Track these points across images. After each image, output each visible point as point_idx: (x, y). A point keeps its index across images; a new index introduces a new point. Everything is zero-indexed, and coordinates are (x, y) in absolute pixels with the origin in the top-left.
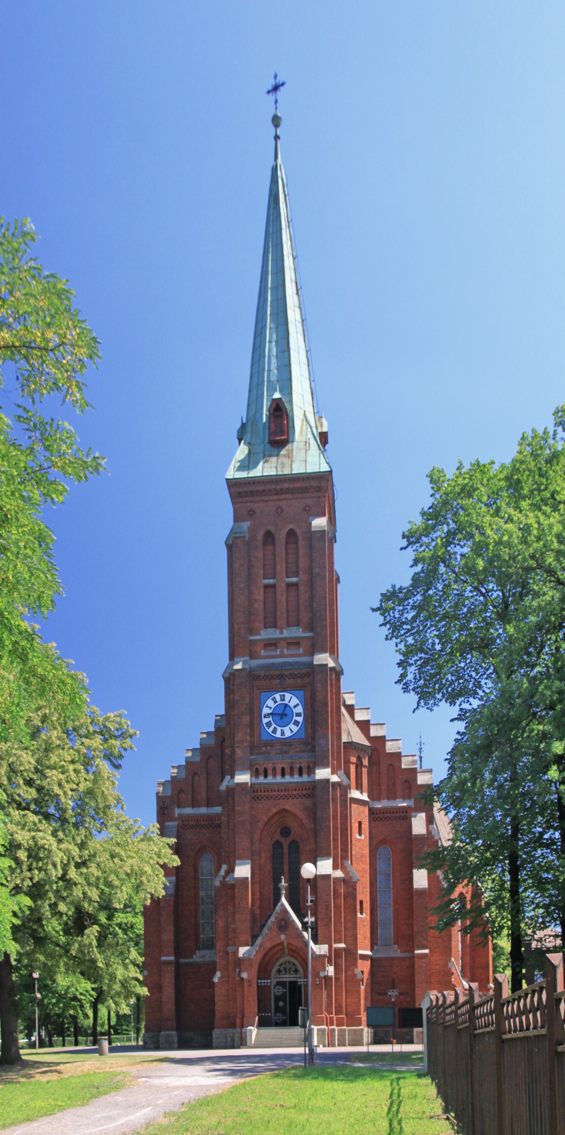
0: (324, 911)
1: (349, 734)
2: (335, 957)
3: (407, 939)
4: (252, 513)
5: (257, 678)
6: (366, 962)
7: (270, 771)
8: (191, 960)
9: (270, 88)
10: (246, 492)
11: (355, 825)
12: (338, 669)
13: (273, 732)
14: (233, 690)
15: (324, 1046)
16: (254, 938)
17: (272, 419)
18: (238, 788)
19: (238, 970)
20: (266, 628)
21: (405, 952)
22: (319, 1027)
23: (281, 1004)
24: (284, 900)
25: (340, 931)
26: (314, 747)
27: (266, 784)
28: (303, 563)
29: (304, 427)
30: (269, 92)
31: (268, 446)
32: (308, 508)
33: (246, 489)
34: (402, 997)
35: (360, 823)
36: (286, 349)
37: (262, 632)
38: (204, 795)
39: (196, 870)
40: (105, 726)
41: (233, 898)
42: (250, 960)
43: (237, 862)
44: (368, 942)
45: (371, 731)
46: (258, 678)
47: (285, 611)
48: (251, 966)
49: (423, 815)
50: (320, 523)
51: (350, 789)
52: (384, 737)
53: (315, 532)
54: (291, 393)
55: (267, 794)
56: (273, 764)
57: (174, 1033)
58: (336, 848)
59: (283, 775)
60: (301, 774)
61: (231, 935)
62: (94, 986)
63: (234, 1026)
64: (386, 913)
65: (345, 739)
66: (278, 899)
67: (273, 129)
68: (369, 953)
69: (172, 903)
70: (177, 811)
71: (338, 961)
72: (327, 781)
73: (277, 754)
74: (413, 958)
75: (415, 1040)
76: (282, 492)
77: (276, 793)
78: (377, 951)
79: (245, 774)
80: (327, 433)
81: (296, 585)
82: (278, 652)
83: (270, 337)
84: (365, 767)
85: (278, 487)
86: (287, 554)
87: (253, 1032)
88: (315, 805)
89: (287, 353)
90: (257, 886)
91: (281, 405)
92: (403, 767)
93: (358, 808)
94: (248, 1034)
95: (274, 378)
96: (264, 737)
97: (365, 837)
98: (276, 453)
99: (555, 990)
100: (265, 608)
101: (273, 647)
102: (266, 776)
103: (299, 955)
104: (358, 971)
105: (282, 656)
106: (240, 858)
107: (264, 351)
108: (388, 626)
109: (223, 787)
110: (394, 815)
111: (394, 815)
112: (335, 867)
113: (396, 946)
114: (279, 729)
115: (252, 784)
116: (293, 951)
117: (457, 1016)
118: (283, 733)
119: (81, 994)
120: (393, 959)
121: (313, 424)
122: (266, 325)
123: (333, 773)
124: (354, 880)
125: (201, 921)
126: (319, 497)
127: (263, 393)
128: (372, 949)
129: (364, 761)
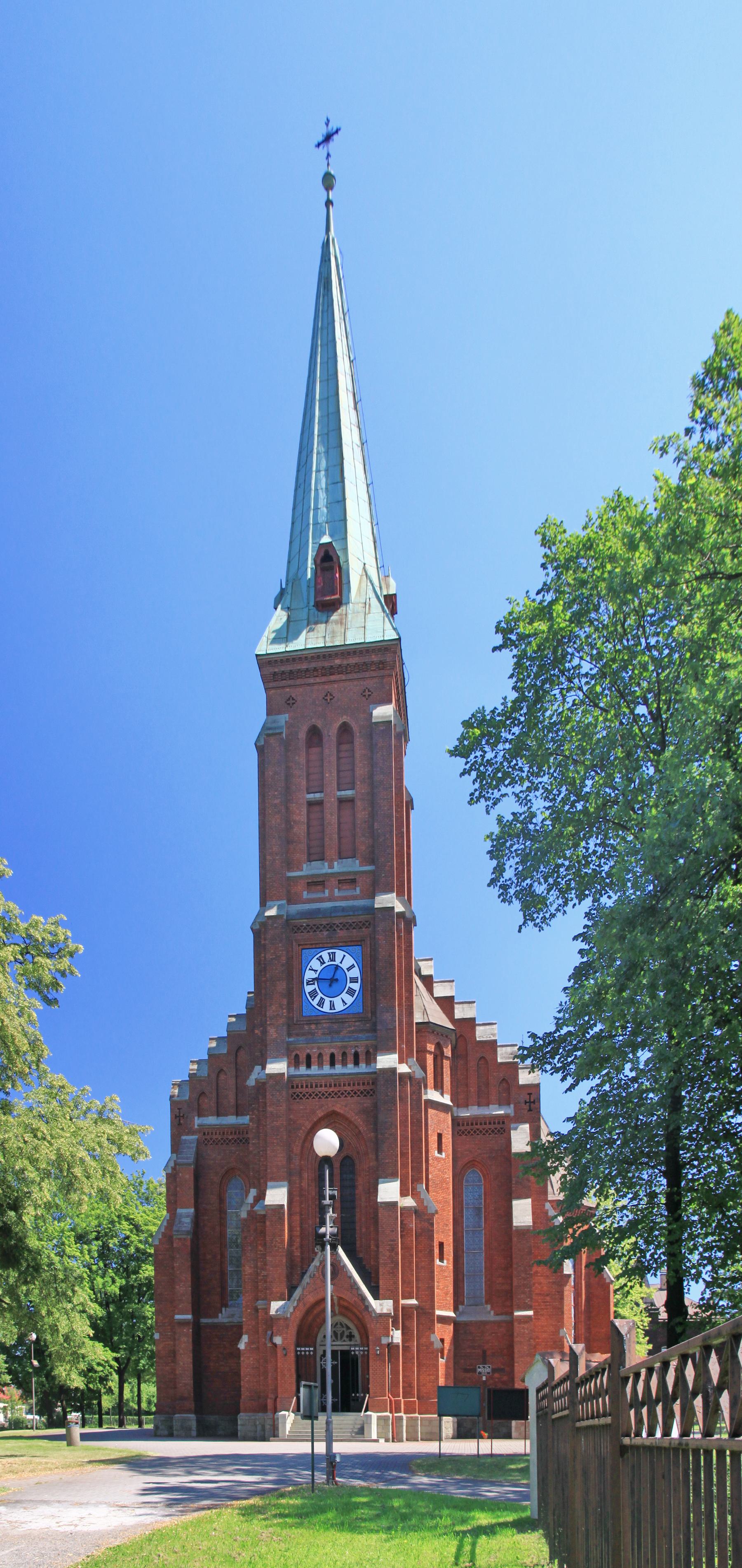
0: (388, 1254)
2: (403, 1317)
3: (504, 1297)
4: (291, 701)
5: (297, 929)
6: (447, 1326)
7: (314, 1059)
8: (216, 1321)
9: (321, 139)
10: (283, 673)
11: (433, 1139)
12: (408, 915)
14: (265, 945)
15: (387, 1440)
16: (292, 1289)
17: (319, 571)
18: (271, 1082)
19: (269, 1333)
20: (310, 861)
21: (502, 1314)
22: (379, 1414)
25: (411, 1282)
26: (375, 1024)
27: (308, 1076)
28: (361, 770)
29: (364, 585)
30: (318, 145)
31: (314, 610)
32: (367, 693)
33: (283, 669)
34: (496, 1375)
35: (440, 1136)
36: (339, 479)
37: (305, 866)
38: (232, 1101)
39: (222, 1200)
40: (30, 936)
41: (263, 1233)
42: (286, 1319)
43: (269, 1184)
44: (450, 1299)
45: (456, 1011)
46: (299, 929)
47: (336, 836)
48: (287, 1326)
49: (526, 1127)
50: (384, 712)
51: (426, 1087)
52: (474, 1019)
54: (345, 539)
55: (310, 1090)
56: (319, 1048)
58: (404, 1165)
59: (332, 1064)
60: (356, 1063)
61: (261, 1285)
62: (115, 1355)
64: (476, 1261)
65: (418, 1018)
67: (325, 193)
69: (189, 1243)
70: (197, 1121)
71: (407, 1323)
72: (393, 1070)
73: (324, 1034)
74: (510, 1323)
75: (514, 1434)
76: (332, 671)
77: (323, 1089)
78: (462, 1313)
79: (279, 1062)
80: (395, 595)
81: (351, 801)
83: (318, 464)
84: (447, 1058)
85: (326, 664)
86: (339, 758)
87: (289, 1420)
88: (375, 1106)
89: (339, 468)
90: (297, 1218)
91: (331, 553)
92: (499, 1060)
93: (437, 1115)
94: (280, 1421)
95: (322, 519)
97: (447, 1156)
98: (324, 619)
100: (309, 834)
101: (319, 887)
102: (309, 1066)
103: (354, 1314)
104: (435, 1338)
105: (331, 899)
106: (273, 1179)
107: (310, 484)
108: (474, 774)
109: (251, 1082)
110: (487, 1127)
111: (487, 1127)
112: (403, 1193)
113: (489, 1307)
115: (290, 1077)
116: (347, 1308)
117: (573, 1404)
118: (332, 1006)
119: (99, 1364)
120: (484, 1323)
121: (376, 583)
122: (312, 451)
123: (401, 1061)
124: (431, 1211)
125: (229, 1269)
126: (383, 677)
127: (308, 540)
128: (455, 1310)
129: (445, 1050)
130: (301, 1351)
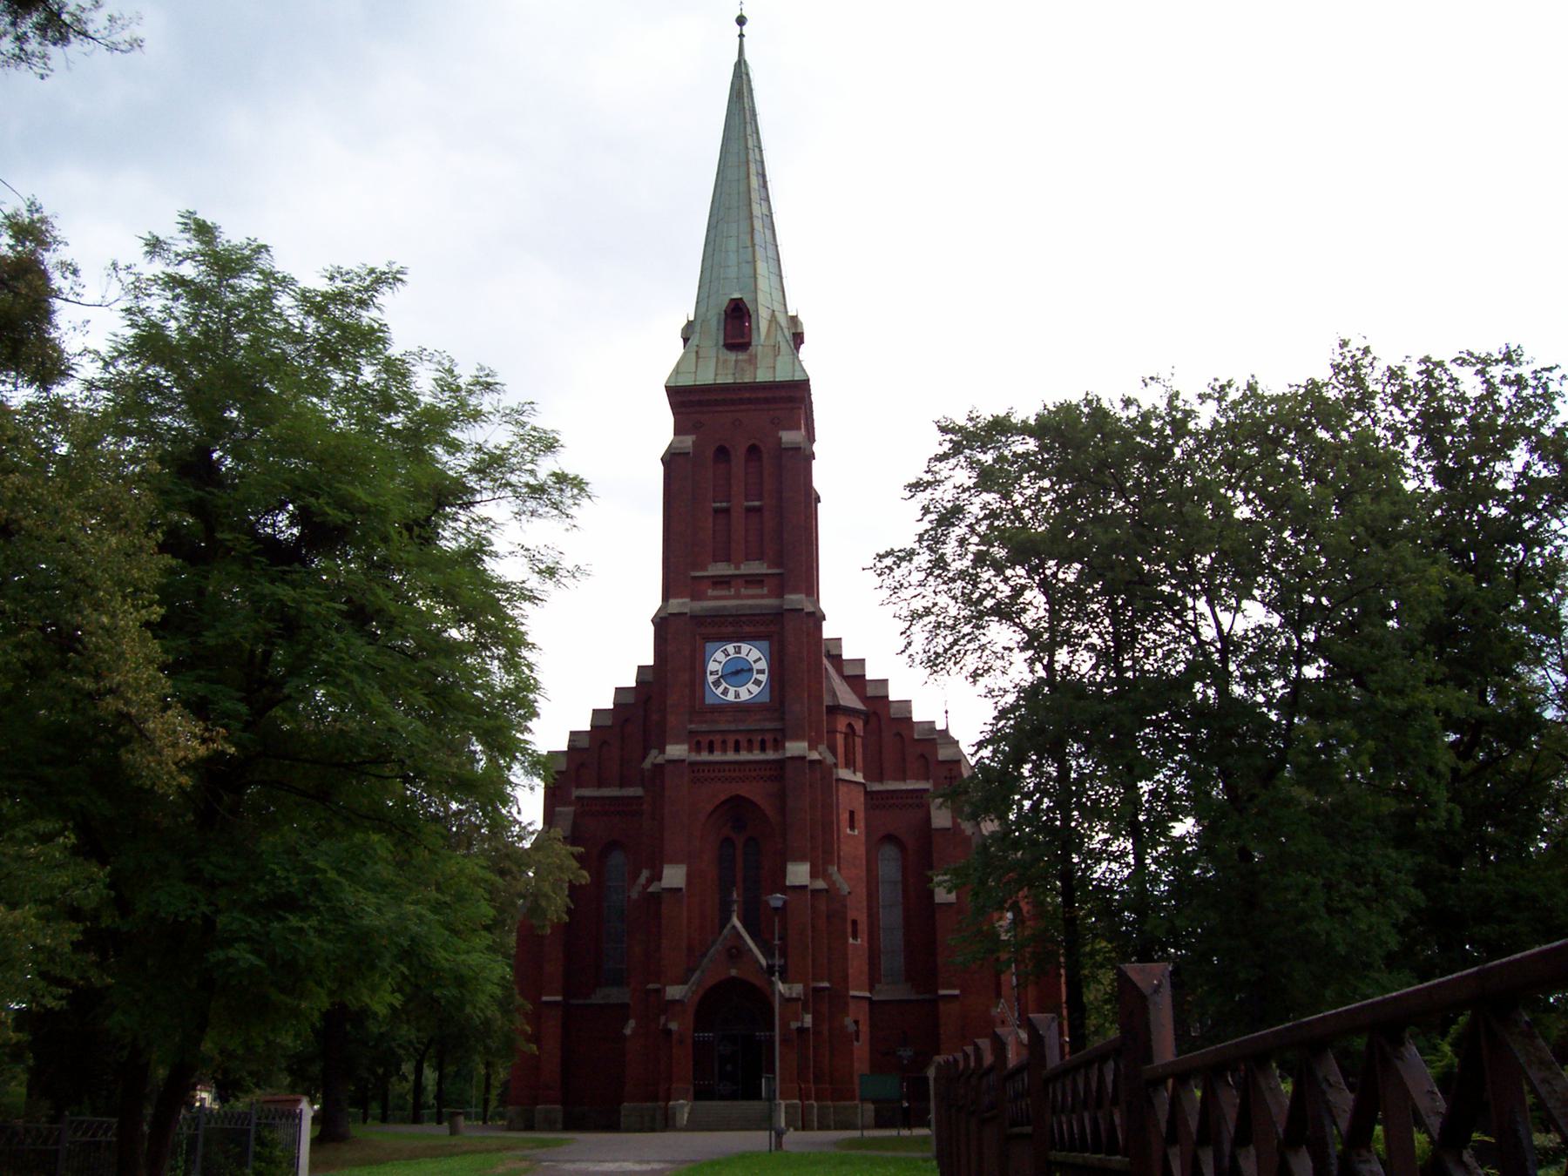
1: (834, 695)
11: (846, 816)
23: (729, 1067)
24: (736, 921)
35: (852, 813)
57: (558, 1107)
63: (656, 1098)
65: (827, 701)
66: (729, 919)
68: (867, 994)
70: (576, 792)
81: (758, 510)
96: (709, 700)
99: (1147, 1053)
106: (671, 862)
109: (647, 764)
114: (732, 690)
118: (737, 695)
119: (400, 1046)
123: (812, 747)
128: (871, 989)
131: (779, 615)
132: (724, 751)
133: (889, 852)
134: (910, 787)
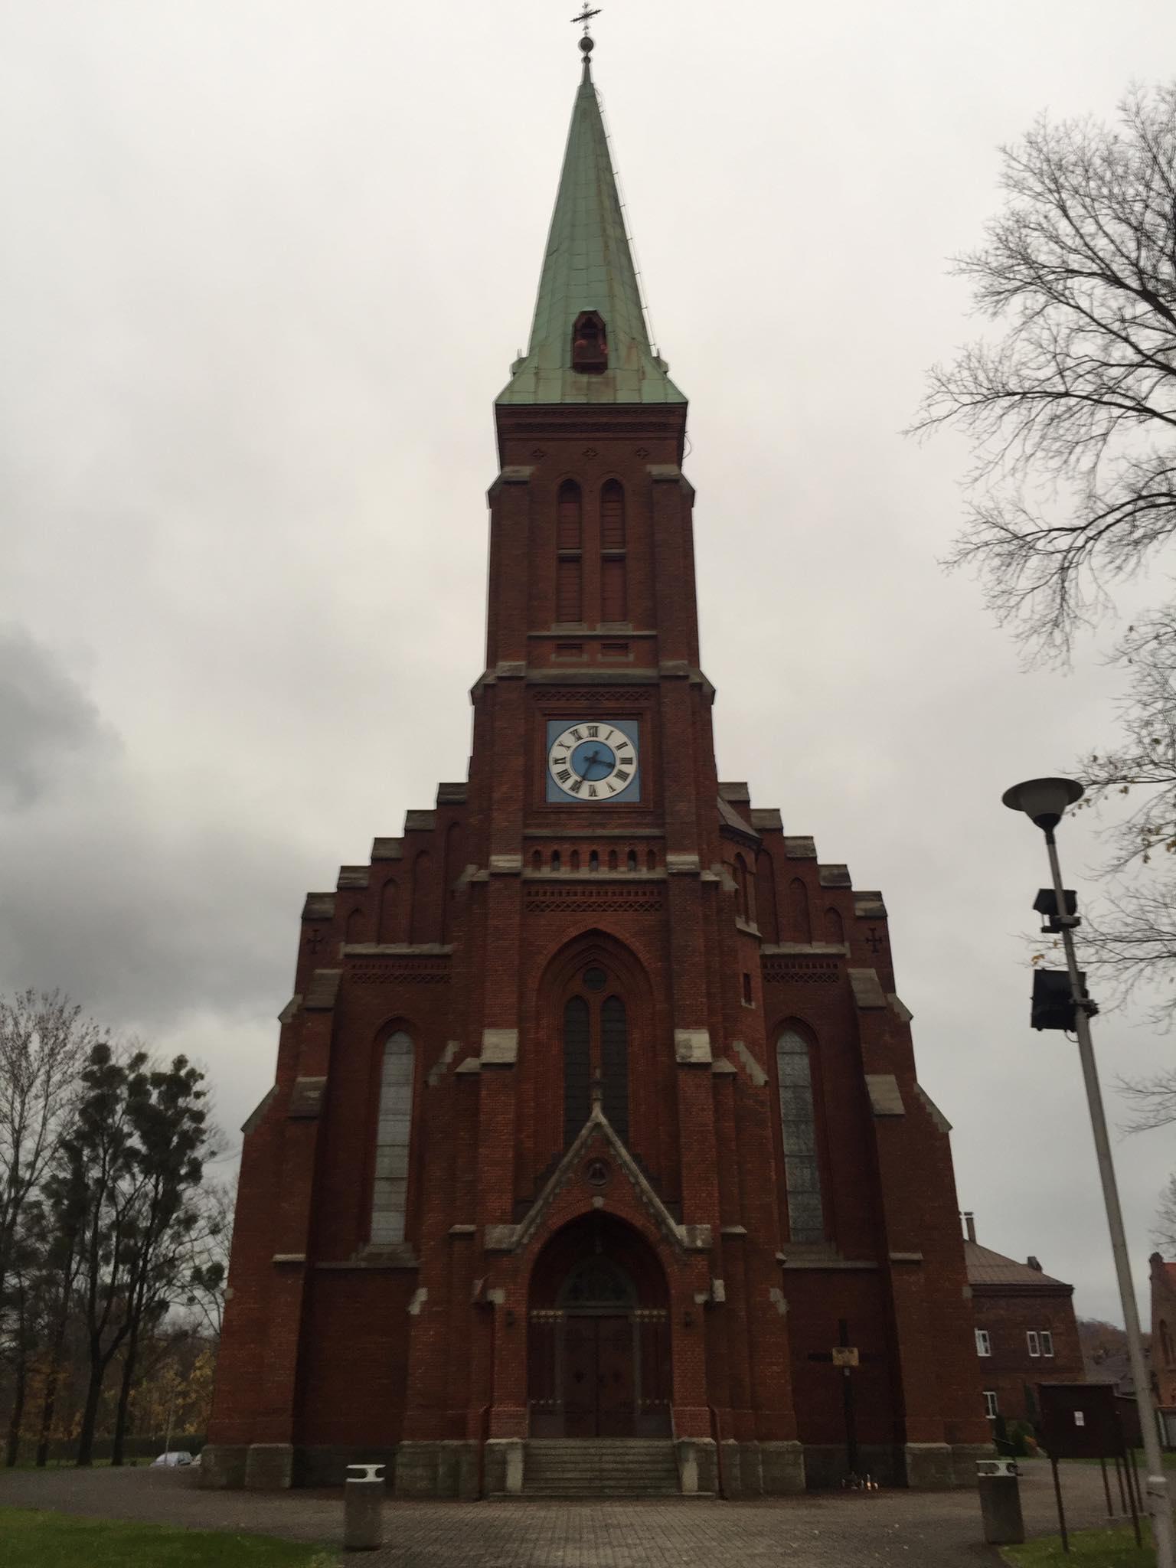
13: (572, 788)
24: (598, 1115)
53: (511, 1027)
63: (458, 1429)
81: (620, 559)
82: (585, 658)
96: (553, 798)
106: (493, 1025)
130: (539, 1317)
131: (649, 689)
132: (575, 865)
133: (790, 1042)
134: (819, 951)
